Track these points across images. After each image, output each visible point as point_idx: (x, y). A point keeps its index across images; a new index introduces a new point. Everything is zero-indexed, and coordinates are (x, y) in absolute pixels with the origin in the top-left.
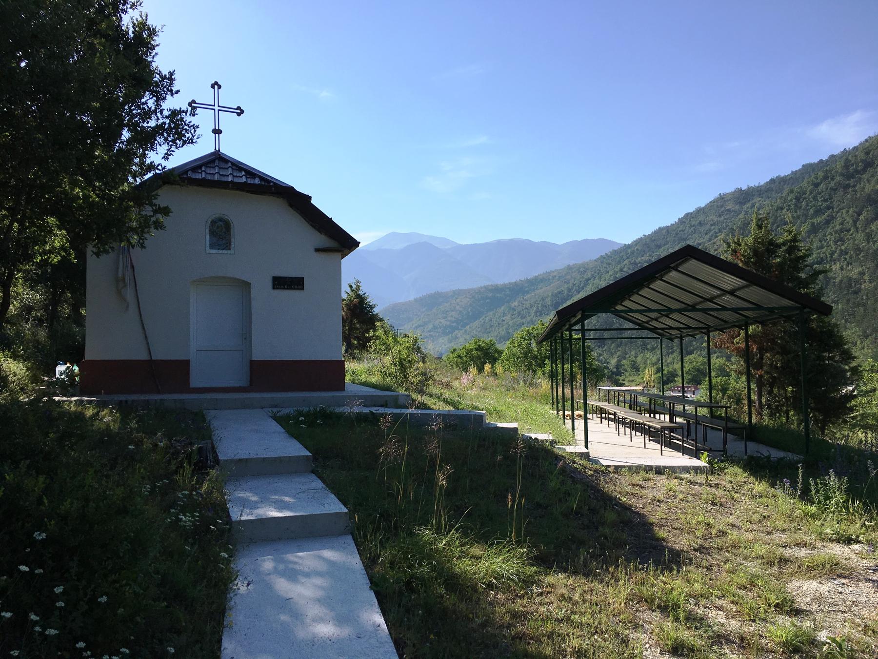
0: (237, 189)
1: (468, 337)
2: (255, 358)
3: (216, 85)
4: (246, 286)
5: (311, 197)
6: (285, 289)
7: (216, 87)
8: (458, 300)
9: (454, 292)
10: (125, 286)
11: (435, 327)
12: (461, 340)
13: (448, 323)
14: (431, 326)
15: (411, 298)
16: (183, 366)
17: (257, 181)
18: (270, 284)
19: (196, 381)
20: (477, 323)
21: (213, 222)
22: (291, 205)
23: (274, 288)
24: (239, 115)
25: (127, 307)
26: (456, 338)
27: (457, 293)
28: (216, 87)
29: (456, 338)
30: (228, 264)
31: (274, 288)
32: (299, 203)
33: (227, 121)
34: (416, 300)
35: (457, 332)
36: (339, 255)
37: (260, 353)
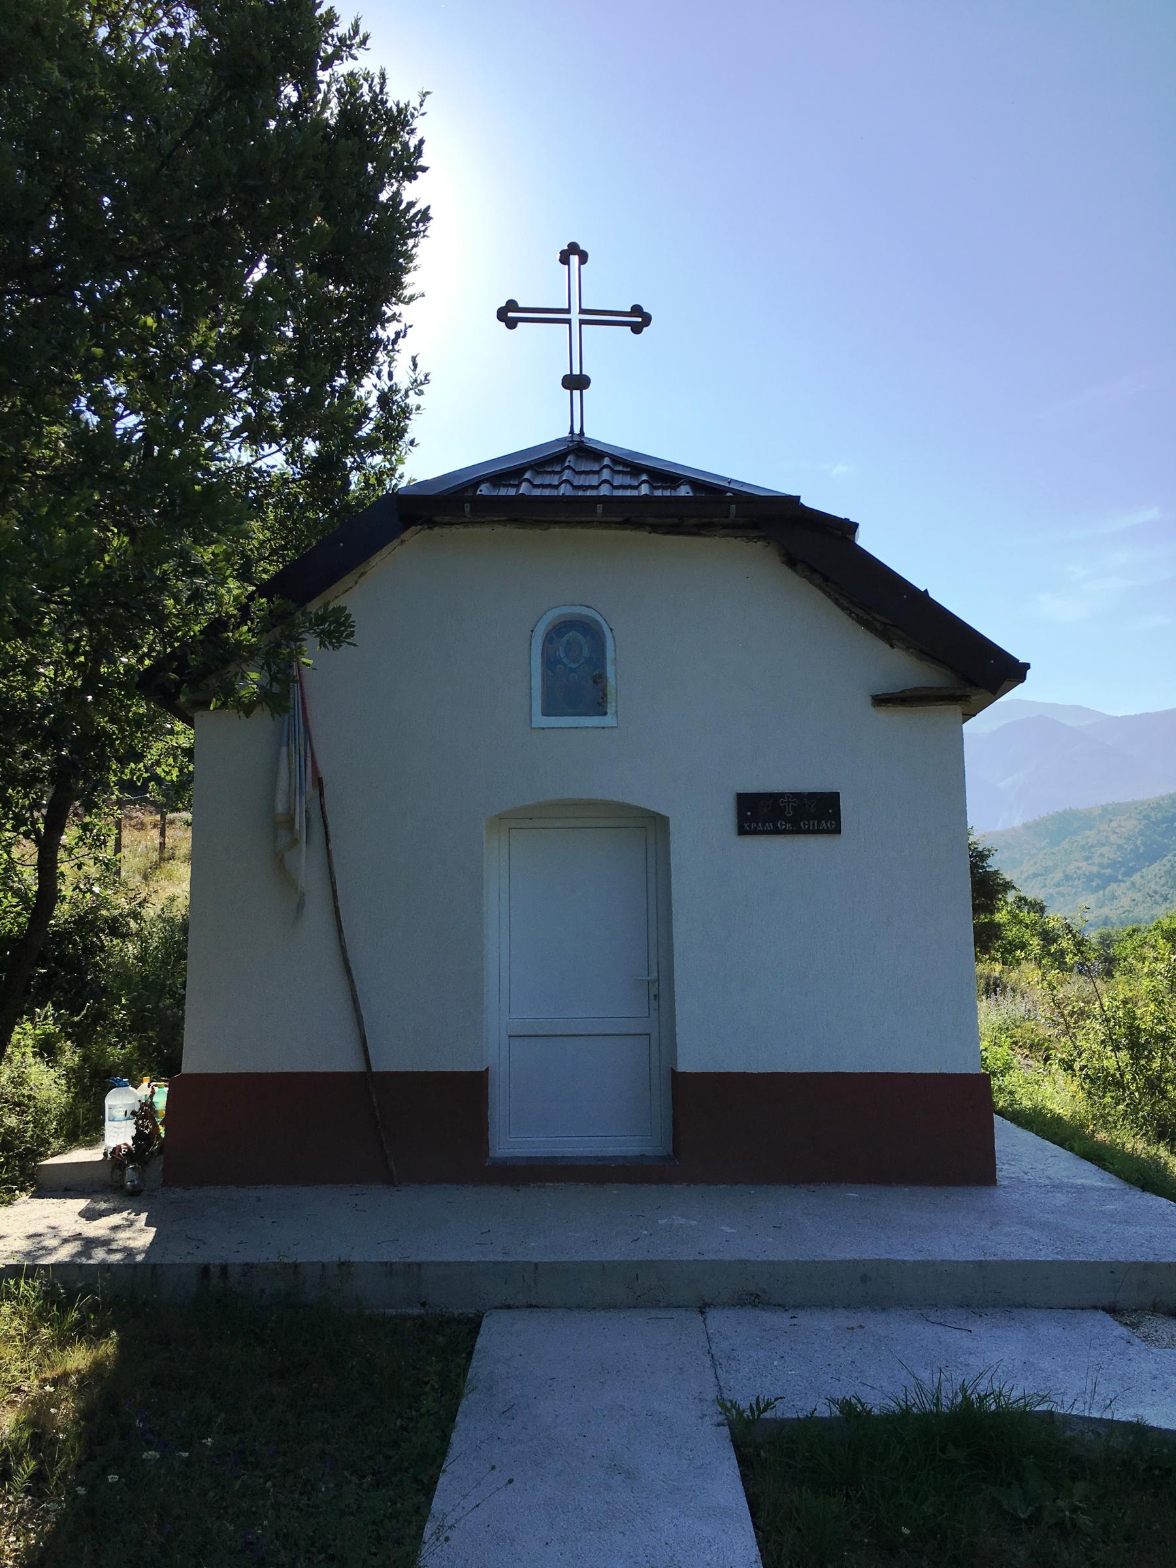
0: (628, 523)
1: (1138, 896)
2: (683, 1066)
3: (572, 252)
4: (653, 827)
5: (851, 527)
6: (777, 832)
7: (575, 259)
8: (1114, 824)
9: (1104, 808)
10: (295, 842)
11: (1068, 878)
12: (1125, 902)
13: (1095, 869)
14: (1059, 875)
15: (1017, 822)
16: (465, 1094)
17: (684, 491)
18: (727, 815)
19: (509, 1139)
20: (1157, 868)
21: (559, 629)
22: (791, 562)
23: (742, 831)
24: (637, 329)
25: (300, 906)
26: (1114, 897)
27: (1109, 812)
28: (575, 259)
29: (1114, 897)
30: (602, 758)
31: (742, 831)
32: (812, 546)
33: (604, 348)
34: (1026, 826)
35: (1113, 886)
36: (957, 710)
37: (710, 1044)
